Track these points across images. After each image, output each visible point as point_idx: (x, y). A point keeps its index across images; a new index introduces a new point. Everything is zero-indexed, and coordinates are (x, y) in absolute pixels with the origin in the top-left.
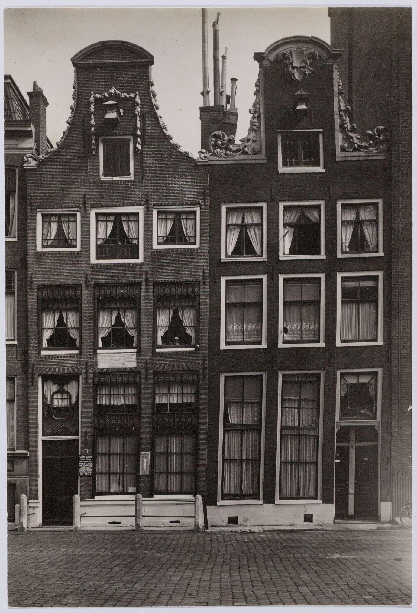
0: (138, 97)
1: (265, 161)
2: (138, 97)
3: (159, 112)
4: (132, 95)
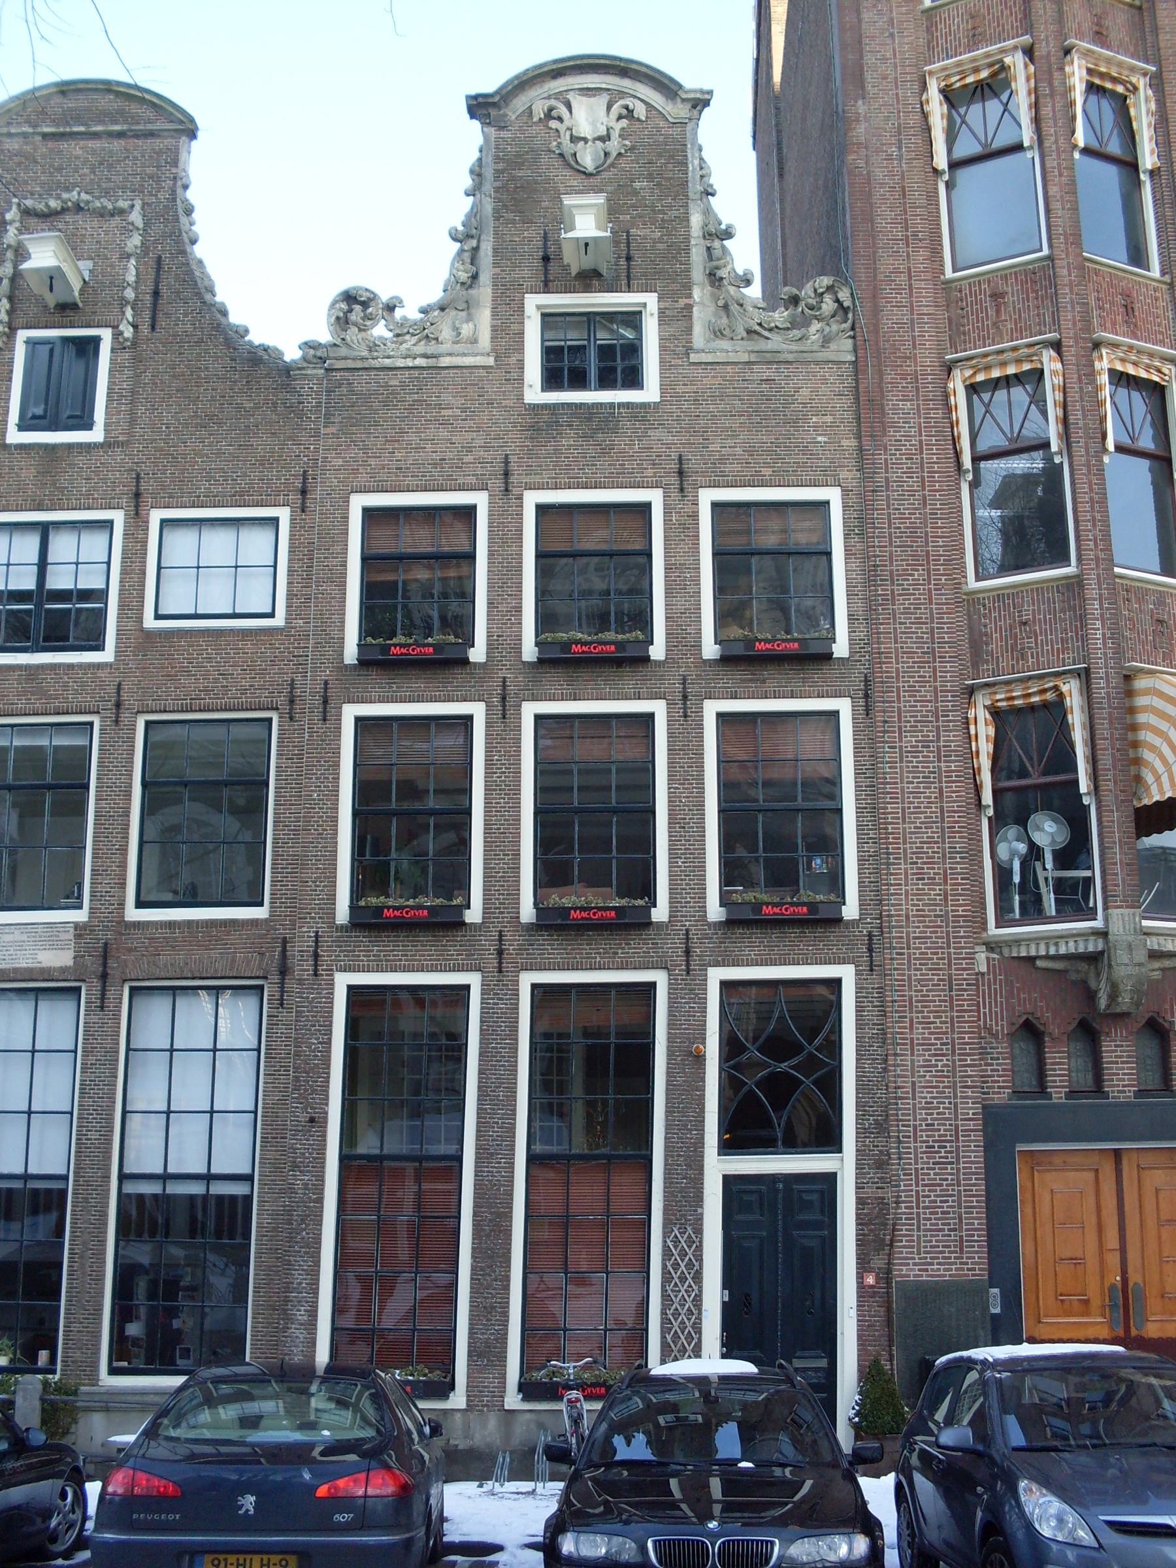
0: (138, 207)
1: (490, 361)
3: (199, 251)
4: (123, 204)
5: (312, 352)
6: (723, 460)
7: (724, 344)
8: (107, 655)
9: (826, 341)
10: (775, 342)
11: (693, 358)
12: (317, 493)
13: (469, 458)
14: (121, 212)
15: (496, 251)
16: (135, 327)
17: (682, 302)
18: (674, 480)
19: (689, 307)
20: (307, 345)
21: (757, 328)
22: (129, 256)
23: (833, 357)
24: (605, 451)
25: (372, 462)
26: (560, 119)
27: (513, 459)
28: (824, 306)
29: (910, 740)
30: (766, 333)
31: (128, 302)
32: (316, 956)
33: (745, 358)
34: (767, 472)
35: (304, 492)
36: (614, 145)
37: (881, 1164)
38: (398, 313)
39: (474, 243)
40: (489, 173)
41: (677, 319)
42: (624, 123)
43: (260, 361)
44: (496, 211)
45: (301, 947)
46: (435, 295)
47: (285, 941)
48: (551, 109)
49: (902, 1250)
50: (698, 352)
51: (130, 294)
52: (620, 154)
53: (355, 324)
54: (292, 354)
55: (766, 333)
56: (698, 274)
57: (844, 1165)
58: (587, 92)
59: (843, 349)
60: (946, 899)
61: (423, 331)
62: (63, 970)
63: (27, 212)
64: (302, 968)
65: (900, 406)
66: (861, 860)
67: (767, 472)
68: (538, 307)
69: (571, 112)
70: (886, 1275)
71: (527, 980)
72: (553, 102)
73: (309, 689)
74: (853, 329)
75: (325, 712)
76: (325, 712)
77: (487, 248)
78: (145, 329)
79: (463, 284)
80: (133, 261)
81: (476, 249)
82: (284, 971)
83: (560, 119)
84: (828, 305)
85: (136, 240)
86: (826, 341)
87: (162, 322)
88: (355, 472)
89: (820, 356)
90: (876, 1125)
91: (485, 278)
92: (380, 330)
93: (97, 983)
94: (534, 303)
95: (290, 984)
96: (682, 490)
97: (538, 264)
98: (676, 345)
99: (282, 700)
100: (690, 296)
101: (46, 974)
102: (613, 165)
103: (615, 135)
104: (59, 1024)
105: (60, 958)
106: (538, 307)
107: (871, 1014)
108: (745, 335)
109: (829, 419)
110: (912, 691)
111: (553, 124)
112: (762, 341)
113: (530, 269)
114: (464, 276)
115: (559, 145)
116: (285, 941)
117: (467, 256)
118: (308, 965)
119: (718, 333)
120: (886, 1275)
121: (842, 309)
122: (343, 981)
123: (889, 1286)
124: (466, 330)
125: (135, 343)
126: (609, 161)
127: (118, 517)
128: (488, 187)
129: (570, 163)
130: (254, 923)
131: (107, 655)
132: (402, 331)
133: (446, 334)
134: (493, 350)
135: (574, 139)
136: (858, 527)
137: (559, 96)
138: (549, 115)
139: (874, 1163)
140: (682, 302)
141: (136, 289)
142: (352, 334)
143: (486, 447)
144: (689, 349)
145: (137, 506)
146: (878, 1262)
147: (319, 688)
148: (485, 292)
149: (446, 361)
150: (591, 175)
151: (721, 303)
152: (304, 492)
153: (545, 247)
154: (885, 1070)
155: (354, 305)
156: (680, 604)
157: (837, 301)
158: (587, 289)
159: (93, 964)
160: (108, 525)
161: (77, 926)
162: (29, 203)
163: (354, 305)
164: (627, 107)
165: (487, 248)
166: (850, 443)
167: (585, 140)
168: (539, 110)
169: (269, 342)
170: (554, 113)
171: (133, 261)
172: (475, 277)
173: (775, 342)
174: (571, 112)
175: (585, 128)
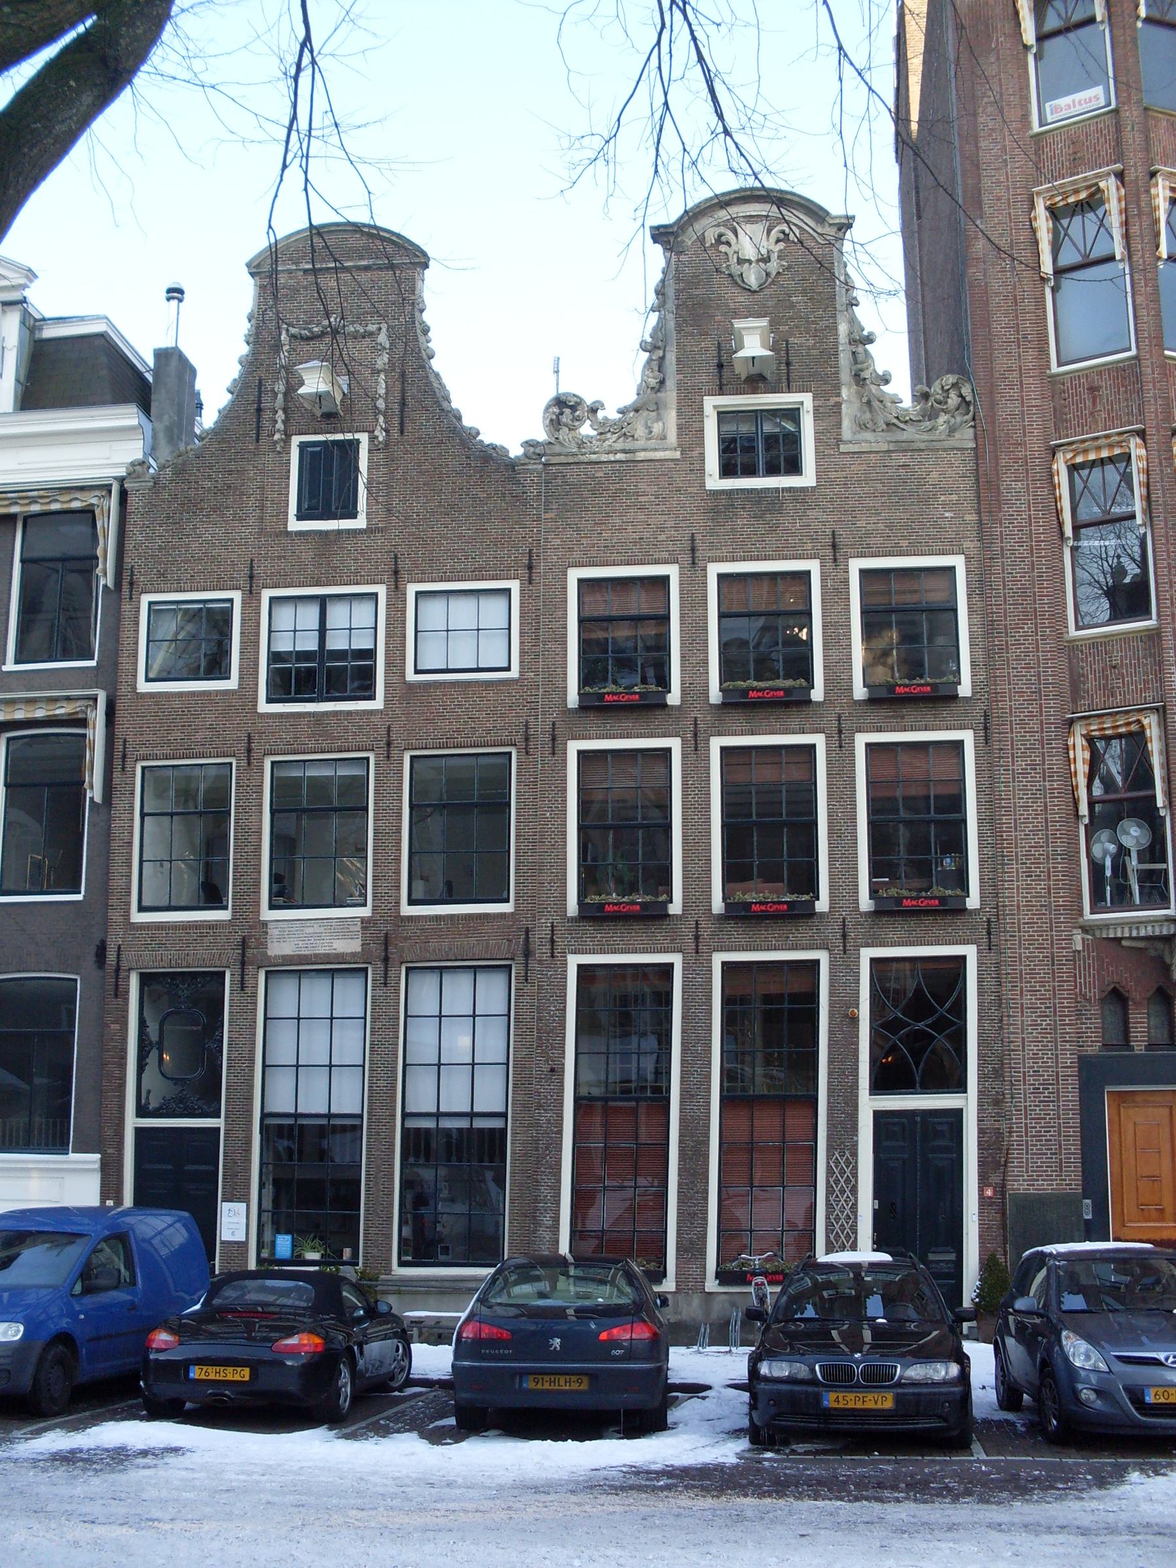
0: (384, 330)
1: (677, 455)
2: (384, 330)
3: (436, 364)
4: (372, 328)
5: (532, 449)
6: (868, 534)
7: (868, 436)
8: (378, 704)
9: (952, 430)
10: (910, 433)
11: (843, 448)
12: (541, 568)
13: (662, 537)
14: (371, 334)
15: (678, 360)
16: (387, 431)
17: (833, 400)
18: (829, 552)
19: (838, 405)
20: (528, 444)
21: (895, 421)
22: (379, 372)
23: (957, 445)
24: (773, 529)
25: (584, 541)
26: (728, 244)
27: (698, 537)
28: (950, 401)
29: (1021, 764)
30: (902, 425)
31: (380, 412)
32: (552, 941)
33: (885, 447)
34: (904, 543)
35: (530, 567)
36: (774, 266)
37: (997, 1102)
38: (600, 414)
39: (661, 353)
40: (671, 292)
41: (828, 414)
42: (781, 245)
43: (489, 459)
44: (678, 325)
45: (540, 935)
46: (629, 397)
47: (527, 931)
48: (720, 235)
49: (1014, 1169)
50: (846, 442)
51: (381, 404)
52: (778, 273)
53: (566, 425)
54: (516, 451)
55: (902, 425)
56: (845, 376)
57: (969, 1103)
58: (751, 219)
59: (966, 437)
60: (1049, 893)
61: (621, 429)
62: (353, 954)
63: (293, 336)
64: (541, 951)
65: (1012, 486)
66: (982, 862)
67: (904, 543)
68: (715, 407)
69: (737, 236)
70: (1001, 1189)
71: (718, 959)
72: (722, 230)
73: (539, 728)
74: (974, 419)
75: (553, 747)
76: (553, 747)
77: (671, 358)
78: (395, 433)
79: (652, 388)
80: (382, 376)
81: (662, 358)
82: (527, 954)
83: (728, 244)
84: (954, 400)
85: (382, 360)
86: (952, 430)
87: (409, 427)
88: (571, 550)
89: (947, 444)
90: (993, 1071)
91: (671, 383)
92: (586, 429)
93: (380, 965)
94: (711, 404)
95: (533, 964)
96: (835, 560)
97: (713, 370)
98: (828, 439)
99: (519, 738)
100: (839, 395)
101: (340, 958)
102: (773, 282)
103: (774, 256)
104: (351, 997)
105: (352, 946)
106: (715, 407)
107: (990, 983)
108: (884, 427)
109: (954, 497)
110: (1022, 723)
111: (723, 248)
112: (899, 432)
113: (706, 376)
114: (653, 382)
115: (728, 267)
116: (527, 931)
117: (655, 365)
118: (546, 949)
119: (863, 427)
120: (1001, 1189)
121: (964, 403)
122: (574, 961)
123: (1004, 1198)
124: (657, 428)
125: (387, 444)
126: (770, 280)
127: (381, 590)
128: (671, 305)
129: (737, 281)
130: (502, 916)
131: (378, 704)
132: (605, 428)
133: (640, 431)
134: (679, 445)
135: (740, 261)
136: (978, 588)
137: (725, 224)
138: (719, 240)
139: (991, 1101)
140: (833, 400)
141: (386, 400)
142: (564, 434)
143: (676, 528)
144: (839, 441)
145: (396, 581)
146: (995, 1178)
147: (548, 728)
148: (671, 395)
149: (641, 456)
150: (755, 292)
151: (865, 400)
152: (530, 567)
153: (719, 356)
154: (1001, 1028)
155: (564, 409)
156: (835, 655)
157: (961, 396)
158: (754, 391)
159: (377, 950)
160: (374, 596)
161: (363, 920)
162: (293, 330)
163: (564, 409)
164: (783, 232)
165: (671, 358)
166: (971, 517)
167: (750, 261)
168: (710, 237)
169: (497, 442)
170: (723, 239)
171: (382, 376)
172: (662, 382)
173: (910, 433)
174: (737, 236)
175: (749, 252)
